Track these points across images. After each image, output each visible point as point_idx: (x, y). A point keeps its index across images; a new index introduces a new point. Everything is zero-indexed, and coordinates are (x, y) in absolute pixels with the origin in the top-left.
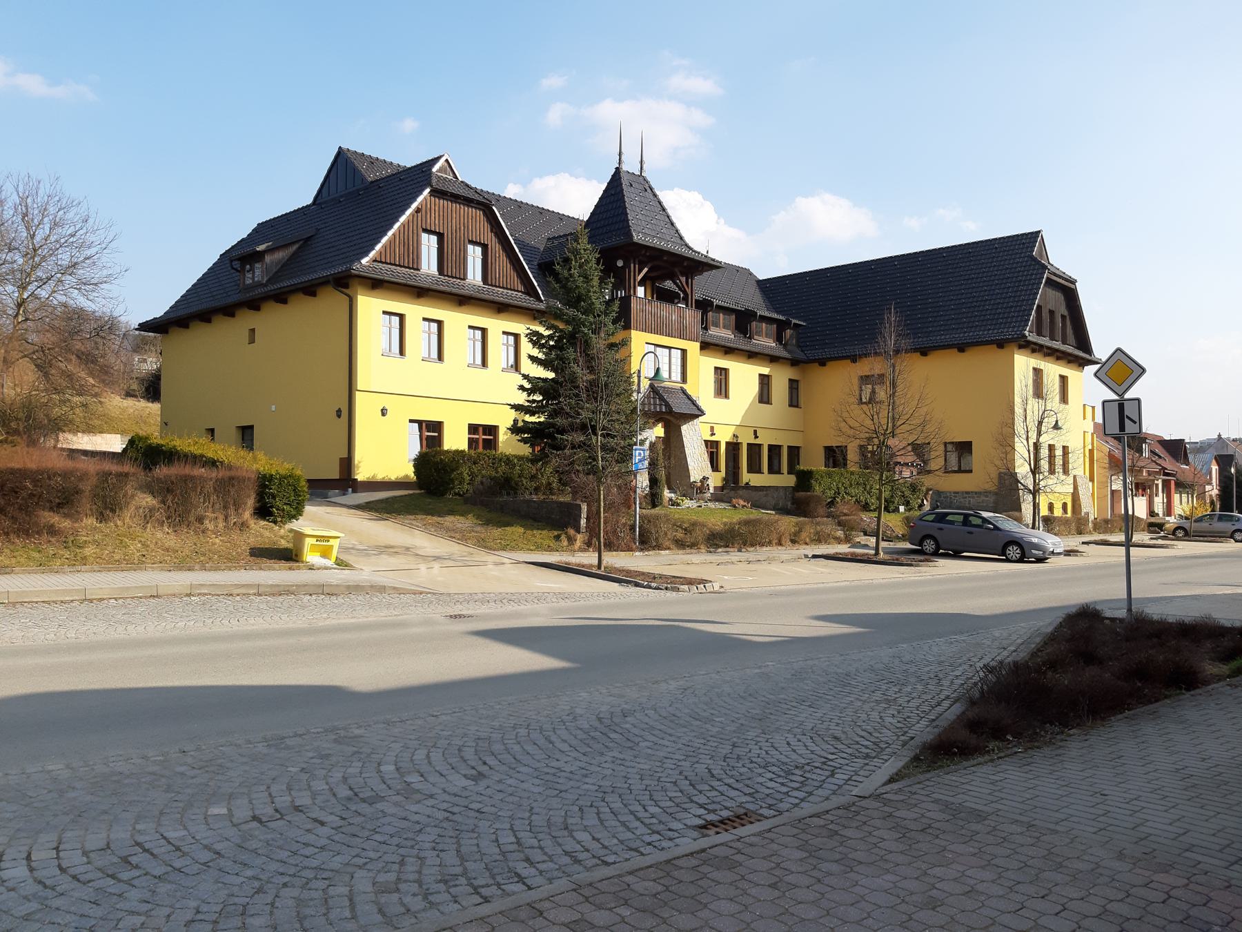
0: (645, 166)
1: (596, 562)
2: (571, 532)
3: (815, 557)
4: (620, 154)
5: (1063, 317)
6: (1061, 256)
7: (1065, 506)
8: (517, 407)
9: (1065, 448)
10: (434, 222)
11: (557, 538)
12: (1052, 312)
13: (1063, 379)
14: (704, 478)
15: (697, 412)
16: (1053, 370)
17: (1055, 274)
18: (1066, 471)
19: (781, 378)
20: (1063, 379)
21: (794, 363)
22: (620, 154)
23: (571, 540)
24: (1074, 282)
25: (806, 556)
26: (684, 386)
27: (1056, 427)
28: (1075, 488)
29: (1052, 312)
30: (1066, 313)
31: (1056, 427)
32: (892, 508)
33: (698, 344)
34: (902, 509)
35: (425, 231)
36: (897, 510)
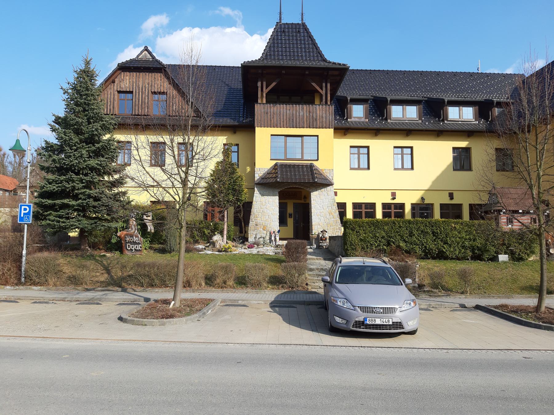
25: (463, 306)
33: (332, 130)
34: (503, 258)
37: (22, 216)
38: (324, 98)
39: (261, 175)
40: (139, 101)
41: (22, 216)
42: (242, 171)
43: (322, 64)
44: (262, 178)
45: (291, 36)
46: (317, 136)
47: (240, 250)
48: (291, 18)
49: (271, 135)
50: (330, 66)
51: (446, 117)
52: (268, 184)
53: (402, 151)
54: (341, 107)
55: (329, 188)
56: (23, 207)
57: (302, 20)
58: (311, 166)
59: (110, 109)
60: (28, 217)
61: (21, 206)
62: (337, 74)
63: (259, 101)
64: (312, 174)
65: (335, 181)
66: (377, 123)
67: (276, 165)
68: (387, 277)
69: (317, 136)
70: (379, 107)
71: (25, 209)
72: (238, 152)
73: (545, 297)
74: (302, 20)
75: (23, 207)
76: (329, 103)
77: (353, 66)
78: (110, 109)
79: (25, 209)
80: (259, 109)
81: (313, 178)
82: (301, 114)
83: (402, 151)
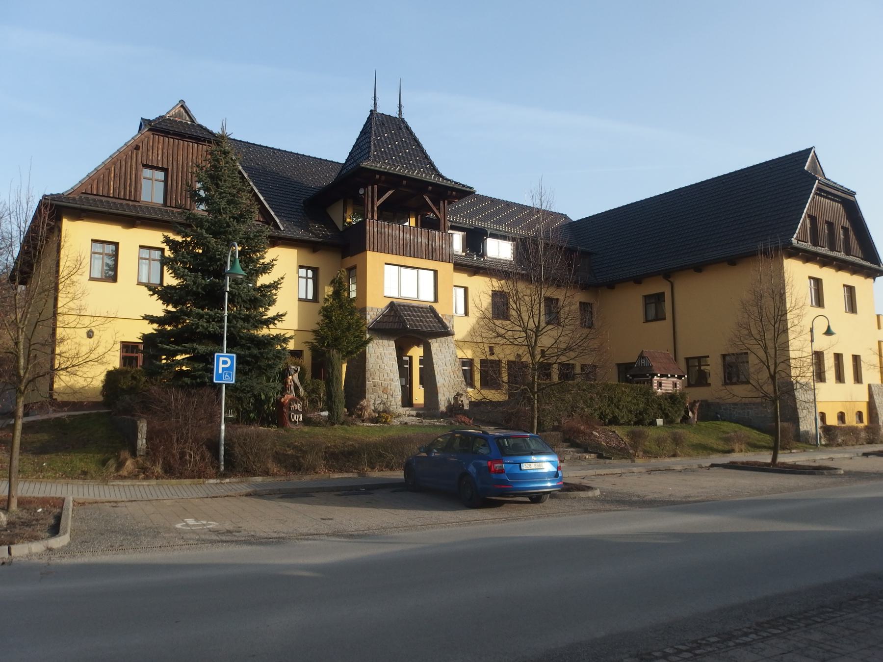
0: (402, 110)
1: (769, 460)
2: (125, 454)
3: (713, 465)
4: (400, 107)
5: (845, 229)
6: (836, 170)
7: (860, 414)
8: (151, 319)
9: (856, 359)
10: (157, 157)
11: (104, 463)
12: (830, 225)
13: (850, 291)
14: (458, 394)
15: (437, 327)
16: (835, 281)
17: (828, 185)
18: (858, 379)
19: (571, 300)
20: (850, 291)
21: (585, 287)
22: (400, 107)
23: (120, 465)
24: (853, 194)
25: (700, 467)
26: (435, 305)
27: (829, 332)
28: (871, 396)
29: (830, 225)
30: (847, 224)
31: (829, 332)
32: (647, 421)
33: (451, 266)
34: (660, 422)
35: (146, 166)
36: (653, 423)
37: (220, 372)
39: (374, 317)
40: (177, 186)
41: (220, 372)
42: (358, 308)
43: (432, 178)
44: (376, 322)
45: (385, 132)
47: (843, 425)
48: (388, 108)
50: (449, 184)
51: (484, 254)
52: (382, 329)
55: (450, 338)
56: (221, 359)
59: (130, 192)
60: (229, 374)
65: (456, 330)
68: (807, 441)
71: (225, 362)
76: (376, 217)
77: (480, 190)
78: (130, 192)
82: (420, 240)
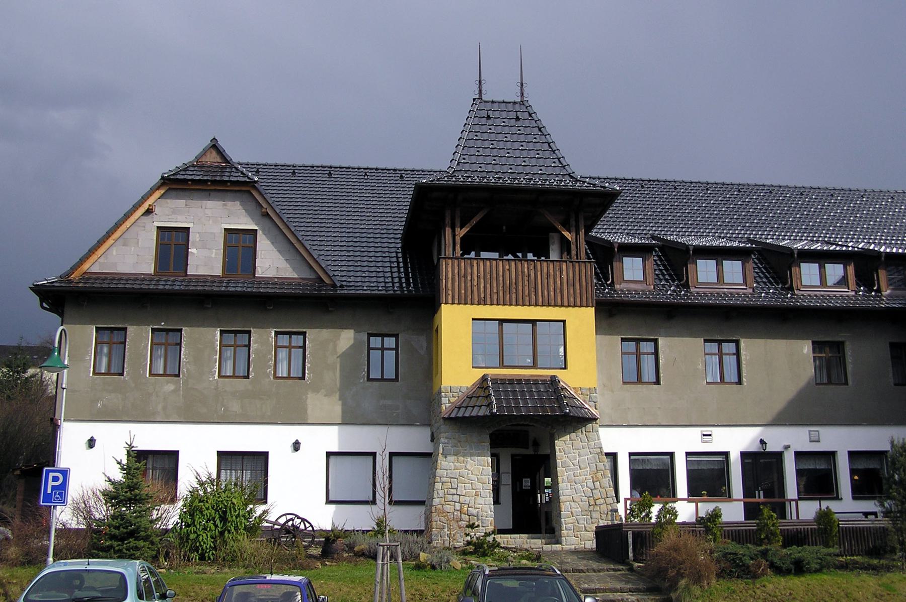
37: (49, 491)
38: (573, 247)
41: (49, 491)
46: (564, 321)
49: (473, 319)
53: (720, 349)
54: (605, 256)
56: (51, 475)
57: (522, 94)
58: (554, 381)
61: (48, 472)
62: (589, 203)
63: (449, 252)
64: (559, 399)
66: (670, 293)
67: (484, 379)
69: (564, 321)
70: (674, 259)
71: (55, 479)
72: (396, 349)
73: (793, 524)
74: (522, 94)
75: (51, 475)
79: (55, 479)
80: (448, 270)
81: (561, 407)
83: (720, 349)
